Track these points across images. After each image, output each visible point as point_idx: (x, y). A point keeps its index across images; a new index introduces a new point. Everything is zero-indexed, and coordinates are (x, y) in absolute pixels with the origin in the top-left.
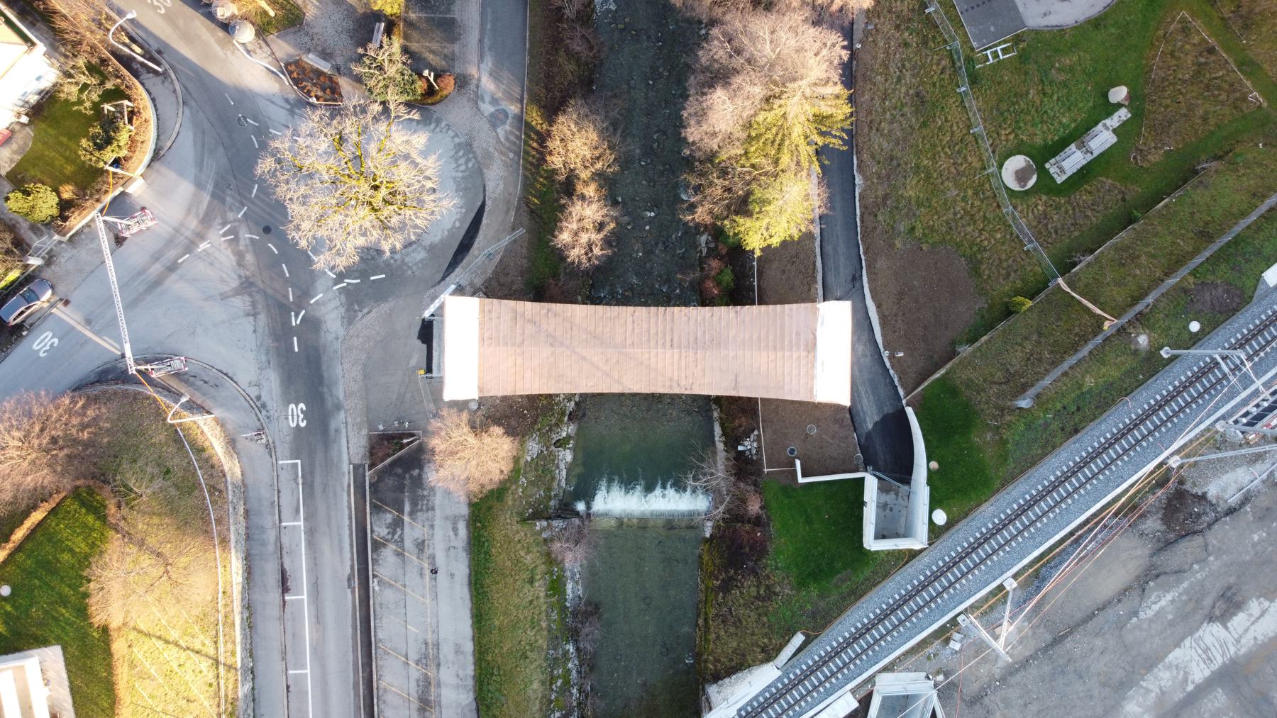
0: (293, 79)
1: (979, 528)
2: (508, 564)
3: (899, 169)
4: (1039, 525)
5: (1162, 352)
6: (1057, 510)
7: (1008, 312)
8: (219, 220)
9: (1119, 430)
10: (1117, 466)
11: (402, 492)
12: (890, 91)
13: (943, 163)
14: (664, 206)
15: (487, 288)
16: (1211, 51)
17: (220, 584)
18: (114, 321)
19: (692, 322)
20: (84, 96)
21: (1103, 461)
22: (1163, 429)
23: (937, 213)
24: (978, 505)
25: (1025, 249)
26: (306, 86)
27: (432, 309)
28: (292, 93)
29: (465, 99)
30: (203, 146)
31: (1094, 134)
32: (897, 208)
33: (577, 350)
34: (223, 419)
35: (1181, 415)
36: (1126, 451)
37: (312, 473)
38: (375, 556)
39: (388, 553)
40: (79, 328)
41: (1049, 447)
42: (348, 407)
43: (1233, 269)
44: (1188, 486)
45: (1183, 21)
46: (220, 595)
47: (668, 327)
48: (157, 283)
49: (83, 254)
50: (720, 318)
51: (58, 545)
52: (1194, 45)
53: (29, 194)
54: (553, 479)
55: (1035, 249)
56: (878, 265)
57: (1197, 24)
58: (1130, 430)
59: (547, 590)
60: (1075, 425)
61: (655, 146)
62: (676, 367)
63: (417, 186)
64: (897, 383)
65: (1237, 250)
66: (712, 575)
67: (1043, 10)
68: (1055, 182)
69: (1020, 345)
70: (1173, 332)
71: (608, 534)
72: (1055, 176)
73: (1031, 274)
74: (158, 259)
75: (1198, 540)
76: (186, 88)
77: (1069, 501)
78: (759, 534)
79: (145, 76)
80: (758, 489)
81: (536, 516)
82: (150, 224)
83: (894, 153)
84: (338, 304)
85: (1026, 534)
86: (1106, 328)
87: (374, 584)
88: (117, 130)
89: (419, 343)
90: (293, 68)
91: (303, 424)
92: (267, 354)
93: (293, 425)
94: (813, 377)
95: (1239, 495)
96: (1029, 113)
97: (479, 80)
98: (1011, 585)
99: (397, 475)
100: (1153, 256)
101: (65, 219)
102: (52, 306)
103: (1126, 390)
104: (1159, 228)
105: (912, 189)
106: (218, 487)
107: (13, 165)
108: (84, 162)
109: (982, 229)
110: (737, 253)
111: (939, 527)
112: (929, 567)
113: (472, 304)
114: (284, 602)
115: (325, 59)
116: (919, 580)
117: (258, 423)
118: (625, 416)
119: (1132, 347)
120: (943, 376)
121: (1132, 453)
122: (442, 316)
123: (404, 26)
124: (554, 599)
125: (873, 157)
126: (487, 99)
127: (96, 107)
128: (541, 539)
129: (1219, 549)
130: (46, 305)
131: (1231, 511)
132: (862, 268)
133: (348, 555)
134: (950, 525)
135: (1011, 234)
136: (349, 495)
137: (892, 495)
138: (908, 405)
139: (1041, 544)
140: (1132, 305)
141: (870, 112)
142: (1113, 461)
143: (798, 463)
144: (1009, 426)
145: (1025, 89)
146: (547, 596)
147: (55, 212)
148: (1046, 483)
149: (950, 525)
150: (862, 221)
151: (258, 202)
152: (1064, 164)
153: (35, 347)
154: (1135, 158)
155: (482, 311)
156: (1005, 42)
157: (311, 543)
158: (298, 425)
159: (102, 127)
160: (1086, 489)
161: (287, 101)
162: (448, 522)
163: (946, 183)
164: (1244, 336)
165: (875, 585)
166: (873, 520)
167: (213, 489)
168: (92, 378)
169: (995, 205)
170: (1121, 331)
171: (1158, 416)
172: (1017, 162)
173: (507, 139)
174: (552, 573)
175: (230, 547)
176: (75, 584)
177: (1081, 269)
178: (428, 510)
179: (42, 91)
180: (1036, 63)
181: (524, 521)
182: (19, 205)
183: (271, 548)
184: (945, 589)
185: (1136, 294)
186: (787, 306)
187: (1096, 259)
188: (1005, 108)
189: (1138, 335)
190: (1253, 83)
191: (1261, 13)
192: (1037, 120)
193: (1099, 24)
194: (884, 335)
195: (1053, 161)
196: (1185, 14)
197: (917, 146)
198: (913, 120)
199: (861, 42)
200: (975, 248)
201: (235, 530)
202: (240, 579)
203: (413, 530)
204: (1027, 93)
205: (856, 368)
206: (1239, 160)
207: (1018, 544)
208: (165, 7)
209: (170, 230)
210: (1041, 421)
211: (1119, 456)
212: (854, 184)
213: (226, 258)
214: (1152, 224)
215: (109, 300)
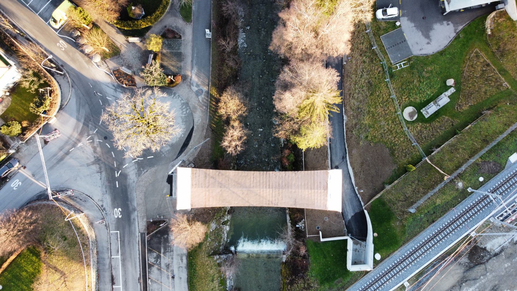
0: (116, 77)
2: (203, 274)
4: (418, 260)
5: (468, 190)
6: (426, 254)
7: (405, 170)
8: (86, 134)
10: (450, 236)
11: (160, 244)
12: (357, 81)
13: (380, 110)
14: (266, 126)
15: (194, 161)
16: (488, 65)
17: (87, 283)
21: (444, 234)
22: (469, 221)
24: (394, 252)
25: (413, 145)
26: (121, 80)
27: (172, 171)
28: (116, 82)
30: (80, 104)
31: (441, 98)
33: (231, 189)
34: (88, 215)
36: (453, 230)
37: (124, 237)
38: (149, 270)
39: (155, 269)
40: (30, 178)
41: (422, 228)
42: (139, 210)
43: (497, 156)
44: (479, 244)
45: (476, 53)
46: (87, 287)
47: (268, 180)
48: (62, 159)
49: (31, 147)
50: (289, 176)
51: (21, 269)
52: (481, 62)
53: (9, 126)
54: (221, 238)
55: (417, 145)
56: (353, 152)
57: (482, 54)
59: (219, 284)
60: (433, 219)
61: (263, 102)
62: (271, 196)
63: (166, 124)
64: (361, 200)
66: (285, 278)
67: (420, 48)
68: (425, 117)
69: (411, 185)
70: (473, 181)
71: (244, 260)
72: (425, 115)
73: (415, 155)
74: (61, 150)
75: (483, 266)
76: (73, 81)
77: (430, 250)
78: (305, 262)
79: (56, 76)
80: (305, 244)
81: (215, 253)
82: (58, 136)
83: (360, 106)
84: (134, 168)
86: (445, 179)
87: (149, 282)
88: (45, 99)
89: (167, 184)
90: (116, 73)
91: (120, 217)
92: (106, 188)
93: (116, 217)
94: (326, 200)
95: (499, 248)
97: (191, 77)
98: (407, 284)
99: (159, 237)
100: (464, 149)
101: (24, 135)
102: (19, 169)
103: (453, 205)
104: (467, 137)
105: (367, 121)
107: (3, 112)
109: (395, 137)
110: (295, 147)
111: (378, 261)
112: (373, 277)
113: (188, 171)
114: (113, 288)
115: (129, 69)
116: (412, 250)
117: (102, 216)
118: (251, 211)
119: (456, 187)
120: (379, 197)
122: (176, 173)
123: (161, 55)
124: (222, 287)
125: (351, 108)
126: (195, 84)
127: (37, 90)
128: (216, 264)
129: (491, 270)
130: (16, 169)
131: (496, 255)
132: (346, 153)
133: (138, 270)
134: (382, 260)
135: (407, 139)
136: (139, 245)
137: (359, 245)
138: (365, 209)
139: (419, 267)
141: (350, 90)
142: (448, 234)
146: (219, 286)
149: (382, 260)
150: (347, 134)
151: (102, 126)
153: (12, 186)
154: (457, 108)
155: (193, 173)
156: (404, 61)
157: (124, 265)
158: (118, 217)
159: (39, 98)
161: (114, 86)
162: (179, 257)
163: (381, 118)
165: (352, 284)
166: (351, 259)
167: (84, 244)
169: (400, 127)
170: (452, 181)
173: (203, 101)
174: (221, 277)
177: (435, 154)
178: (171, 252)
180: (417, 69)
181: (209, 256)
183: (107, 267)
184: (380, 286)
185: (458, 165)
186: (316, 171)
187: (441, 149)
188: (404, 88)
189: (458, 182)
190: (505, 78)
191: (508, 50)
192: (418, 92)
193: (442, 54)
194: (355, 180)
195: (424, 109)
196: (477, 50)
197: (369, 103)
198: (367, 92)
199: (346, 62)
200: (392, 145)
201: (93, 260)
202: (95, 280)
203: (164, 260)
204: (413, 82)
206: (499, 110)
207: (410, 267)
208: (64, 48)
210: (419, 217)
211: (451, 232)
212: (343, 119)
213: (89, 149)
214: (464, 136)
215: (42, 166)
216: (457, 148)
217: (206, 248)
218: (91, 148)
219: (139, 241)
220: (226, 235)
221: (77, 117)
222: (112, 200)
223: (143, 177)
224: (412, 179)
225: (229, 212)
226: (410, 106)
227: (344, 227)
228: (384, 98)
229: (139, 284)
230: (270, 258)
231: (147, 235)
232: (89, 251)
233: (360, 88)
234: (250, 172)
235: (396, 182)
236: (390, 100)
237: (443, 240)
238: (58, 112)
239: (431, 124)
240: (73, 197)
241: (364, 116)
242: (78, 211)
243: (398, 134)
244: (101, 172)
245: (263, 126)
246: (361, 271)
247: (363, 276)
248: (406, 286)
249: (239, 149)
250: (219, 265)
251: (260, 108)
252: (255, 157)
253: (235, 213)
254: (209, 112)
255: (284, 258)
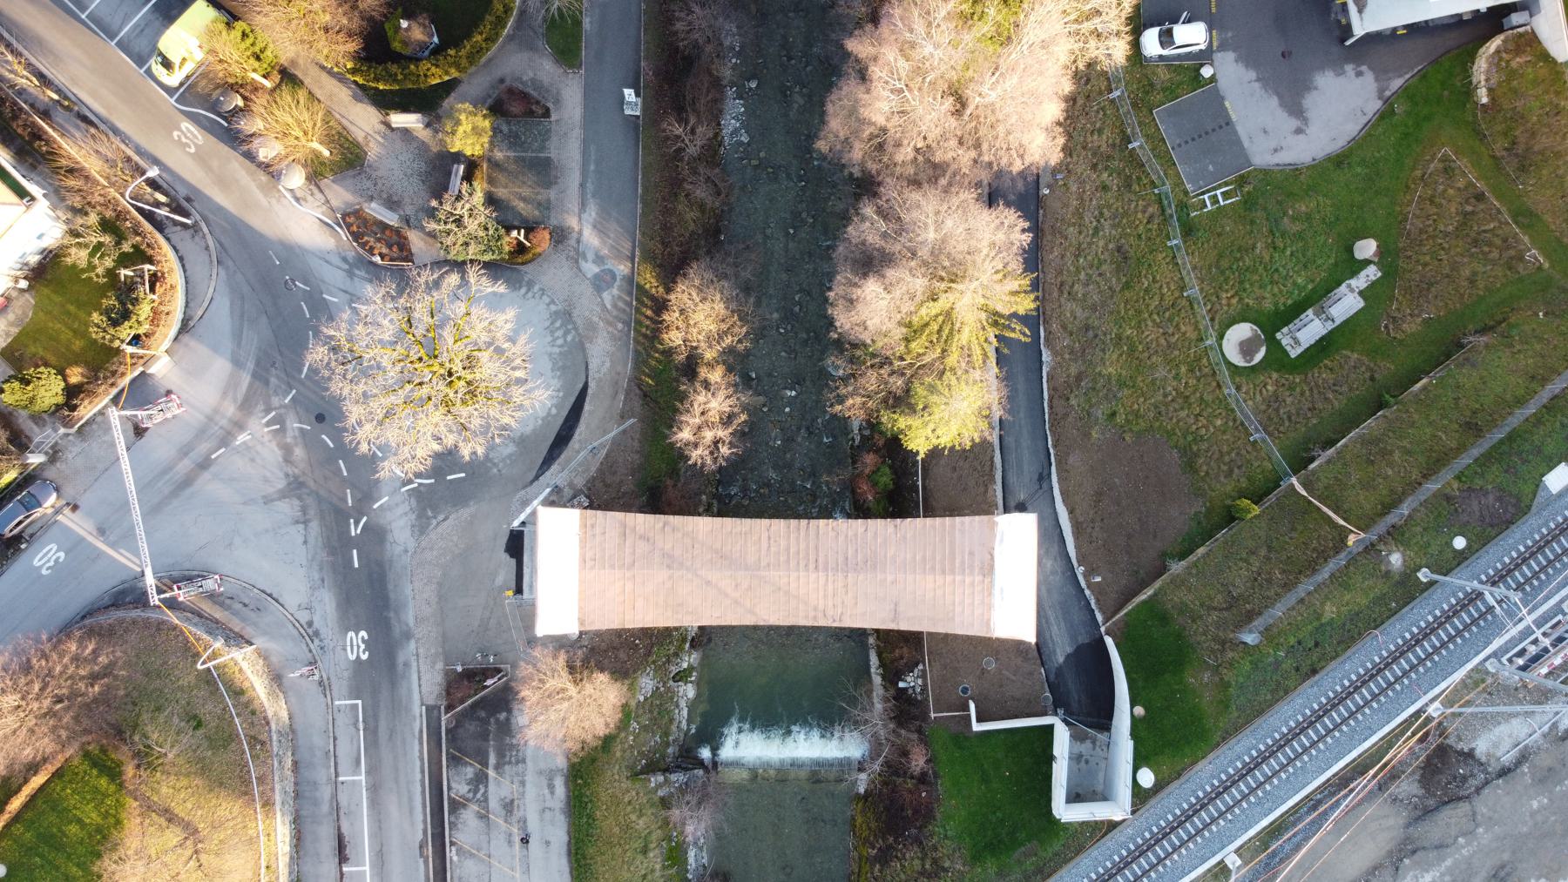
0: (352, 233)
1: (1194, 791)
2: (616, 830)
3: (1097, 340)
4: (1268, 787)
5: (1420, 575)
6: (1291, 770)
7: (1230, 517)
8: (261, 407)
9: (1367, 670)
10: (1364, 714)
11: (486, 739)
13: (1151, 333)
14: (808, 383)
15: (589, 489)
16: (1480, 197)
17: (263, 857)
18: (131, 531)
19: (841, 538)
20: (96, 261)
21: (1347, 709)
23: (1143, 394)
24: (1194, 763)
25: (1251, 439)
26: (367, 242)
27: (522, 517)
28: (352, 249)
29: (563, 257)
30: (242, 316)
31: (1337, 297)
32: (1094, 389)
33: (699, 573)
34: (266, 650)
35: (1444, 652)
36: (1375, 697)
37: (376, 717)
38: (453, 819)
39: (469, 816)
40: (90, 539)
41: (1281, 691)
43: (1506, 471)
44: (1451, 741)
45: (1445, 159)
46: (263, 870)
47: (812, 545)
48: (187, 482)
50: (876, 533)
51: (64, 815)
52: (1459, 189)
53: (28, 383)
54: (671, 720)
55: (1264, 440)
56: (1071, 460)
57: (1462, 163)
58: (1380, 670)
61: (797, 309)
64: (1093, 606)
65: (1511, 448)
66: (866, 841)
67: (1273, 145)
68: (1288, 355)
69: (1246, 561)
70: (1434, 550)
71: (739, 788)
72: (1288, 348)
74: (186, 454)
75: (1464, 807)
76: (221, 244)
77: (1306, 758)
78: (924, 794)
79: (170, 230)
80: (924, 740)
81: (651, 768)
82: (178, 412)
84: (408, 508)
85: (1252, 799)
86: (1350, 543)
87: (452, 854)
88: (136, 301)
89: (506, 557)
91: (364, 657)
92: (321, 569)
93: (352, 657)
94: (990, 607)
95: (1514, 753)
96: (1255, 271)
97: (580, 233)
98: (1233, 861)
99: (478, 719)
100: (1409, 452)
101: (74, 408)
102: (58, 512)
103: (1375, 620)
104: (1416, 417)
105: (1112, 366)
106: (261, 737)
108: (95, 340)
110: (894, 447)
111: (1145, 790)
114: (342, 874)
115: (391, 209)
118: (761, 641)
119: (1383, 568)
120: (1151, 598)
121: (1382, 698)
122: (534, 524)
123: (488, 168)
124: (673, 871)
125: (1064, 327)
126: (590, 256)
127: (111, 274)
128: (656, 799)
129: (1490, 818)
130: (50, 511)
131: (1504, 772)
132: (1050, 464)
133: (420, 817)
134: (1159, 787)
135: (1235, 420)
136: (421, 743)
137: (1088, 744)
139: (1271, 811)
140: (1383, 514)
141: (1060, 273)
143: (972, 706)
144: (1231, 664)
145: (1250, 242)
146: (664, 868)
147: (60, 399)
148: (1277, 736)
149: (1159, 787)
150: (1051, 407)
151: (308, 383)
152: (1299, 335)
153: (36, 563)
154: (1386, 327)
155: (584, 526)
156: (1226, 184)
157: (374, 803)
158: (358, 657)
159: (118, 298)
160: (1326, 743)
161: (345, 260)
162: (543, 778)
163: (1154, 359)
164: (1520, 554)
165: (1067, 861)
167: (254, 740)
168: (107, 601)
169: (1214, 384)
170: (1370, 549)
171: (1415, 653)
172: (1242, 331)
173: (615, 306)
174: (670, 839)
175: (275, 811)
176: (85, 863)
177: (1320, 466)
178: (517, 762)
179: (45, 250)
180: (1265, 209)
181: (635, 775)
182: (16, 397)
183: (325, 808)
184: (1153, 867)
185: (1388, 500)
186: (958, 519)
188: (1226, 266)
189: (1390, 553)
191: (1542, 153)
192: (1267, 280)
195: (1285, 330)
197: (1119, 312)
200: (1190, 438)
201: (281, 788)
202: (287, 848)
203: (499, 788)
204: (1254, 248)
205: (1043, 588)
206: (1514, 332)
207: (1243, 811)
208: (195, 145)
209: (202, 418)
210: (1271, 659)
211: (1367, 703)
212: (1041, 361)
213: (271, 453)
215: (126, 505)
216: (1385, 448)
217: (624, 751)
218: (276, 449)
219: (421, 731)
220: (685, 712)
221: (233, 352)
222: (339, 605)
223: (433, 536)
224: (1251, 544)
225: (695, 644)
226: (1244, 320)
227: (1043, 688)
228: (1166, 298)
229: (421, 861)
230: (818, 781)
231: (446, 713)
232: (269, 761)
233: (1091, 266)
234: (758, 520)
235: (1201, 551)
236: (1184, 302)
237: (1344, 728)
238: (176, 339)
239: (1306, 375)
240: (221, 598)
241: (1103, 350)
242: (237, 639)
243: (1207, 405)
244: (306, 523)
245: (797, 381)
246: (1096, 822)
247: (1103, 837)
248: (1231, 867)
249: (725, 450)
250: (665, 803)
251: (789, 327)
252: (772, 474)
253: (712, 645)
254: (635, 339)
255: (862, 783)
